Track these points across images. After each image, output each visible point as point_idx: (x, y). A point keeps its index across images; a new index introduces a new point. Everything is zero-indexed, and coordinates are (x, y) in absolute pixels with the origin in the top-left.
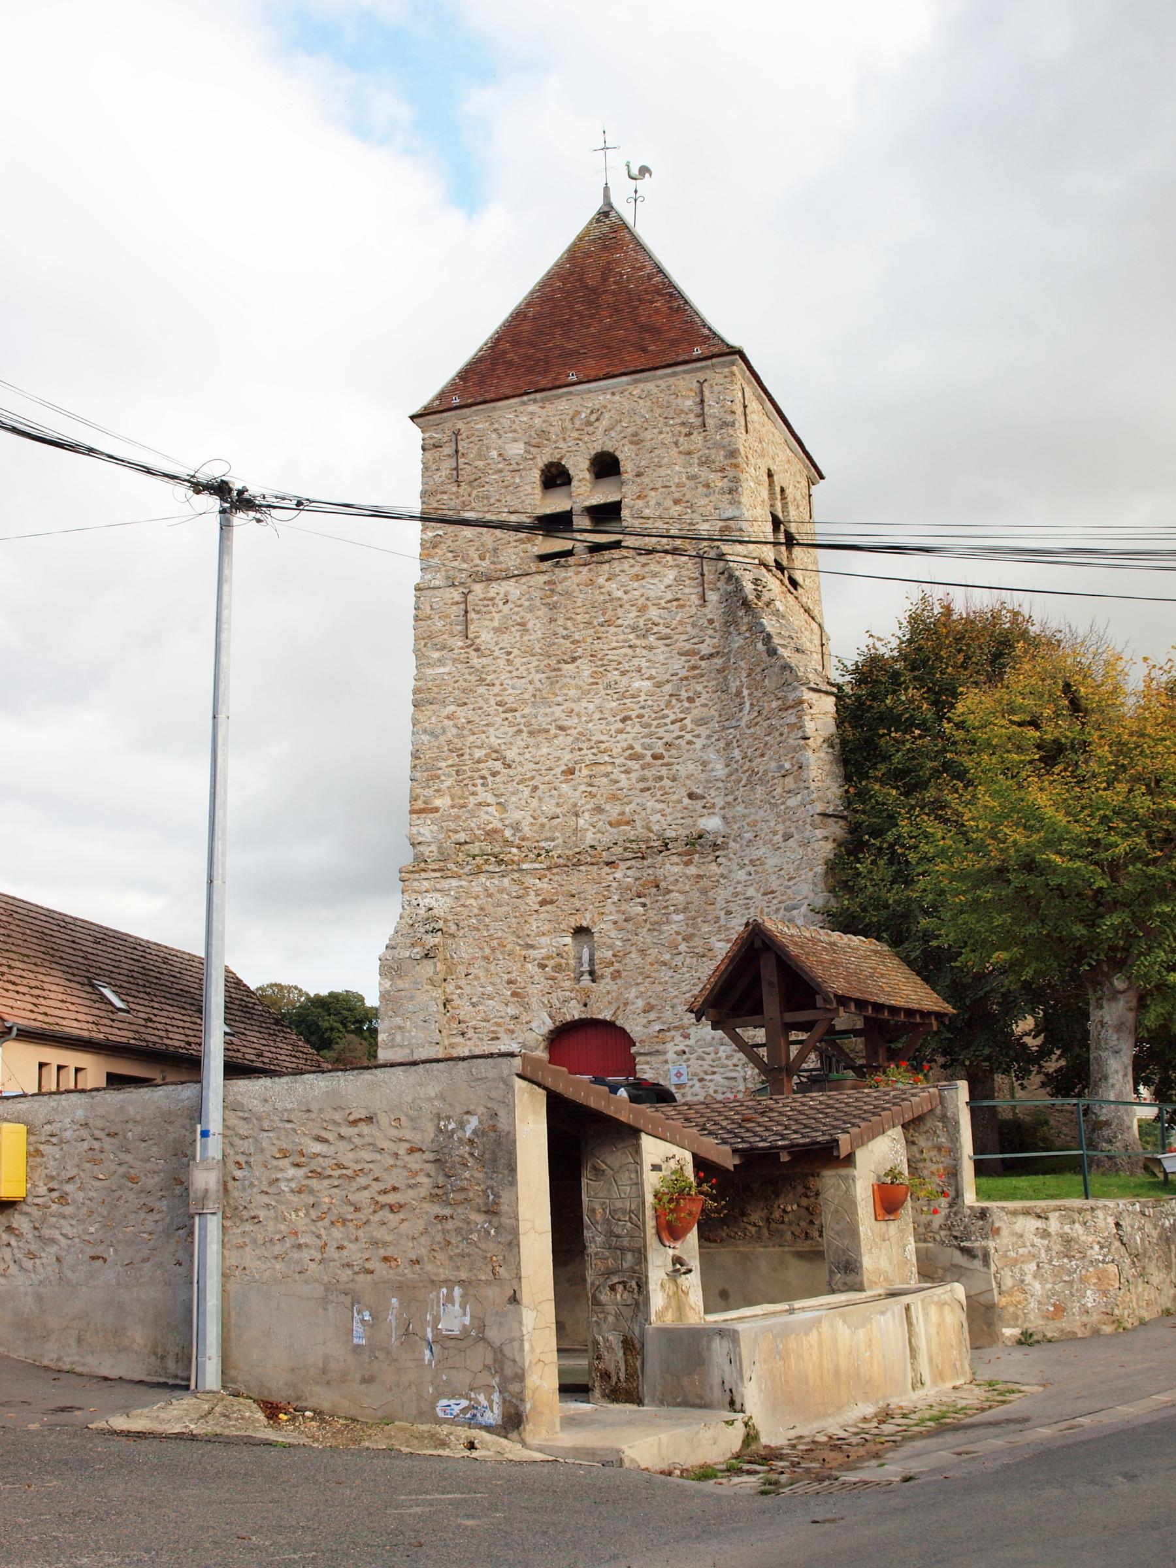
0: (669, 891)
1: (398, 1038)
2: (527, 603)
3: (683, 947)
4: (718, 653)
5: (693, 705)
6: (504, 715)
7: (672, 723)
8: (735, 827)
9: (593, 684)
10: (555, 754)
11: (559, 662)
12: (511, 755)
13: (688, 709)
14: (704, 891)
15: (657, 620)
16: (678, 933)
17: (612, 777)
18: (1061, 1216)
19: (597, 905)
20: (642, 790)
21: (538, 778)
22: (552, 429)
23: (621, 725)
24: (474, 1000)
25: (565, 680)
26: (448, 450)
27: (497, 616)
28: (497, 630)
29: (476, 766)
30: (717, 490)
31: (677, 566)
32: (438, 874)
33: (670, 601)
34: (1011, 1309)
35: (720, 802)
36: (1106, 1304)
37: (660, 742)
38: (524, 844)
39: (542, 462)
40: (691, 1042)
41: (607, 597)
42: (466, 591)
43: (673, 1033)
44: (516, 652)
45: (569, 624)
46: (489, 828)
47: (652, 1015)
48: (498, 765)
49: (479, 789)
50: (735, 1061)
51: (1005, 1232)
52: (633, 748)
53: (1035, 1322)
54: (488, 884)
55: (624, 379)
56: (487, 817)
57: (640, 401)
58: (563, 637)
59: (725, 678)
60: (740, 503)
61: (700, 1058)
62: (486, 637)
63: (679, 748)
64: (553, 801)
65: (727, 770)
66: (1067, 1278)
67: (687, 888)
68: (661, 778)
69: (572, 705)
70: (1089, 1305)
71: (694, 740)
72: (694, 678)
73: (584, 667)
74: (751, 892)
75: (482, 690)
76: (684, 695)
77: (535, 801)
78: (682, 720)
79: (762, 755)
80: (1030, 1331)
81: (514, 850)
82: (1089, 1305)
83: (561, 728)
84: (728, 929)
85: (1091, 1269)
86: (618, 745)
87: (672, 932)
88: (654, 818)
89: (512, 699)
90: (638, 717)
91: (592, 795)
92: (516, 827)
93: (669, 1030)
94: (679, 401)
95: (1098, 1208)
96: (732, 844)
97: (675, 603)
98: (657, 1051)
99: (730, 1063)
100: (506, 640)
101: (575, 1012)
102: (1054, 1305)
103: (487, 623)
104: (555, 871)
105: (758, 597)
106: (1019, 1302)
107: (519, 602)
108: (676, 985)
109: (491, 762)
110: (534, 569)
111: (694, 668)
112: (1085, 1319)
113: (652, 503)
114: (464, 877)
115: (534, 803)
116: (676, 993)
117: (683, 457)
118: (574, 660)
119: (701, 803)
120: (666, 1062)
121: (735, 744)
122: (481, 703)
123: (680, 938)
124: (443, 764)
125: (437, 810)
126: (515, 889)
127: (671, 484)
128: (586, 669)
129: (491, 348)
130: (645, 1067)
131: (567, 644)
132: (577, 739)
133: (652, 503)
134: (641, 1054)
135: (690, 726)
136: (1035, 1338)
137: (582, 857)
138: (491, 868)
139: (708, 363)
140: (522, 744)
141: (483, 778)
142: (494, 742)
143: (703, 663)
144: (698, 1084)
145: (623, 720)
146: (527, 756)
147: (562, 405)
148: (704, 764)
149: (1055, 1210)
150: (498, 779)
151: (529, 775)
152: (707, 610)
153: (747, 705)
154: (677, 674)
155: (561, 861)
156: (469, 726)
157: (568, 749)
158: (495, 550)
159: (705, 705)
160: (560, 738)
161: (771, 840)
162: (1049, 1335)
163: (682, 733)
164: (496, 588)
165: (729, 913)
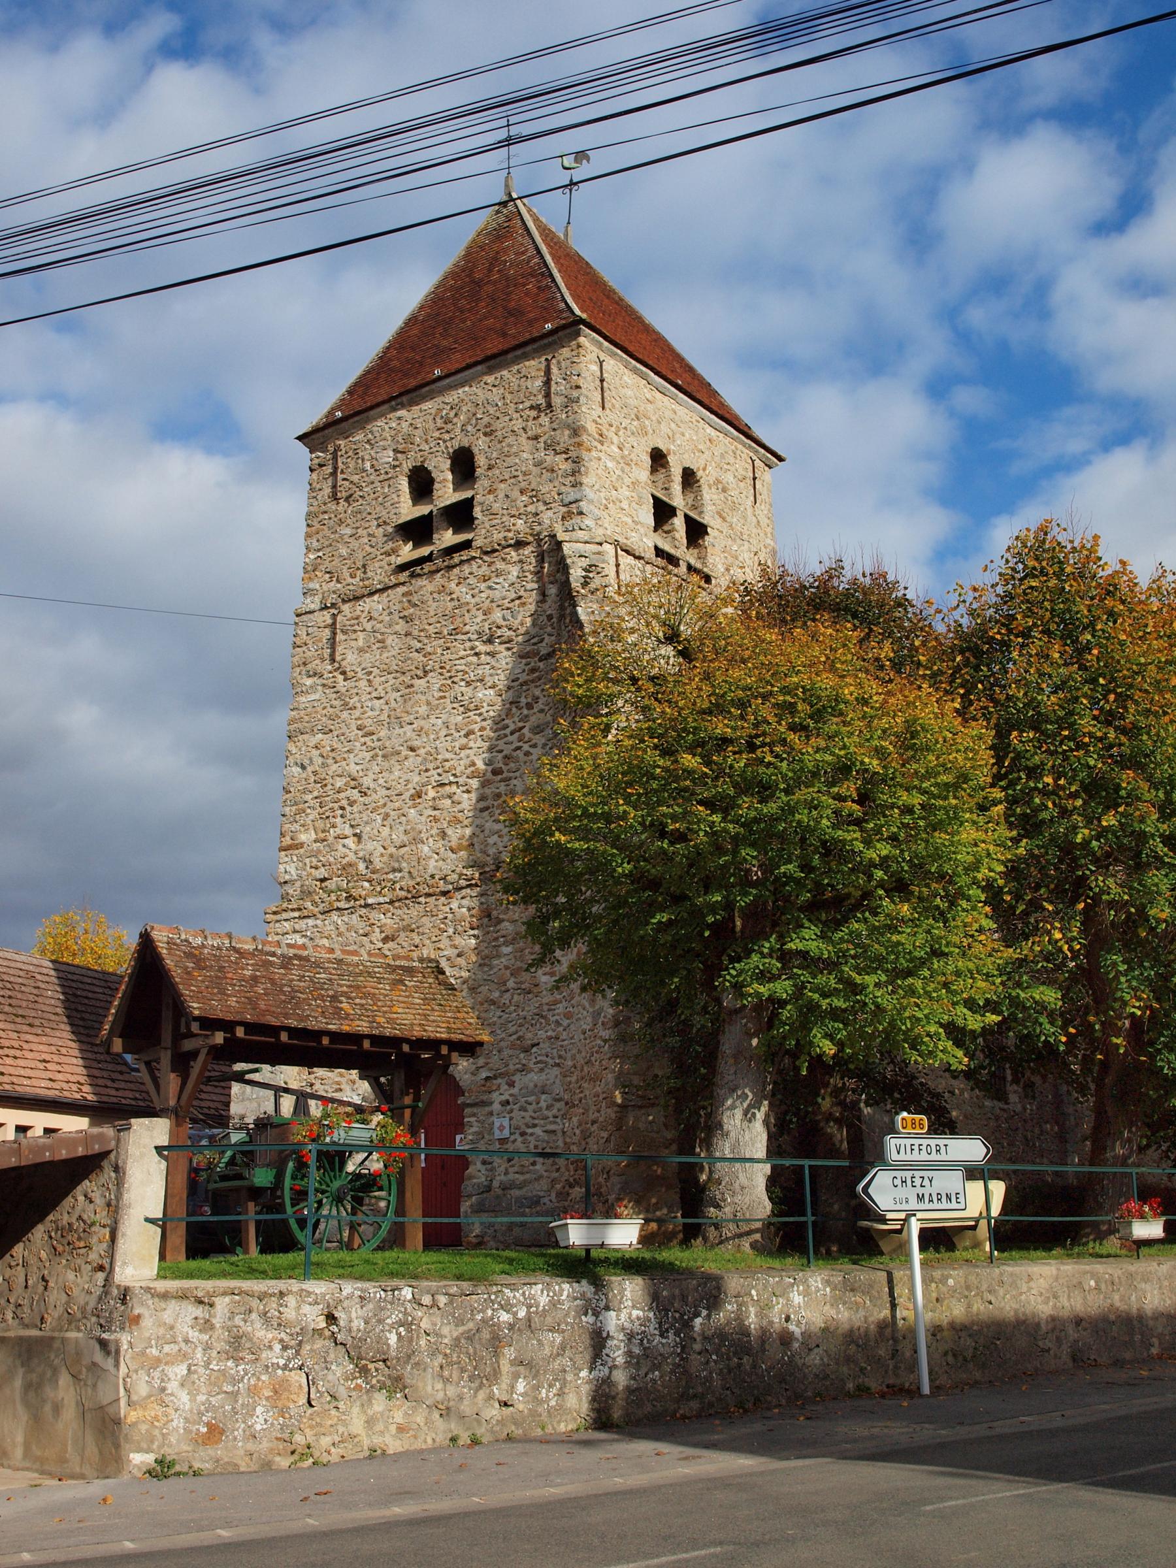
0: (500, 921)
5: (531, 712)
6: (363, 740)
7: (512, 733)
9: (441, 698)
12: (367, 781)
13: (526, 716)
15: (501, 622)
16: (507, 968)
17: (456, 798)
18: (233, 1302)
19: (434, 939)
21: (389, 804)
22: (416, 432)
25: (417, 697)
26: (328, 469)
27: (361, 635)
28: (361, 650)
29: (337, 796)
30: (560, 472)
31: (521, 561)
32: (296, 914)
33: (513, 601)
34: (143, 1428)
36: (283, 1427)
37: (500, 756)
38: (374, 876)
39: (407, 466)
40: (515, 1091)
41: (456, 603)
42: (336, 612)
43: (499, 1081)
46: (344, 861)
49: (339, 820)
50: (555, 1111)
51: (147, 1322)
52: (473, 764)
53: (177, 1446)
54: (339, 922)
55: (479, 368)
56: (344, 850)
57: (494, 389)
58: (417, 651)
60: (581, 484)
62: (350, 659)
64: (402, 829)
66: (230, 1389)
69: (422, 723)
70: (258, 1427)
71: (531, 750)
72: (533, 681)
73: (434, 681)
75: (345, 715)
76: (523, 701)
77: (387, 829)
78: (521, 729)
80: (169, 1458)
81: (366, 884)
82: (258, 1427)
85: (264, 1378)
86: (462, 762)
87: (501, 966)
90: (480, 730)
91: (436, 820)
92: (369, 862)
93: (495, 1077)
94: (529, 384)
95: (290, 1292)
97: (517, 602)
98: (482, 1102)
99: (550, 1114)
102: (208, 1424)
103: (353, 643)
104: (397, 904)
105: (585, 584)
106: (156, 1418)
110: (394, 581)
111: (533, 670)
112: (250, 1446)
114: (320, 916)
115: (386, 831)
116: (503, 1035)
117: (531, 442)
120: (491, 1114)
122: (344, 730)
123: (508, 972)
124: (309, 797)
125: (301, 845)
126: (362, 927)
127: (519, 473)
128: (435, 680)
129: (381, 358)
130: (472, 1119)
131: (419, 657)
132: (425, 759)
133: (501, 495)
136: (177, 1468)
137: (420, 888)
138: (342, 905)
139: (555, 337)
140: (377, 769)
141: (342, 808)
142: (353, 769)
143: (541, 665)
144: (520, 1139)
145: (467, 735)
146: (381, 781)
147: (427, 405)
149: (224, 1294)
150: (355, 808)
151: (382, 802)
152: (546, 606)
154: (517, 679)
155: (403, 894)
156: (333, 755)
157: (417, 770)
158: (364, 566)
159: (542, 711)
160: (411, 759)
162: (197, 1465)
163: (521, 744)
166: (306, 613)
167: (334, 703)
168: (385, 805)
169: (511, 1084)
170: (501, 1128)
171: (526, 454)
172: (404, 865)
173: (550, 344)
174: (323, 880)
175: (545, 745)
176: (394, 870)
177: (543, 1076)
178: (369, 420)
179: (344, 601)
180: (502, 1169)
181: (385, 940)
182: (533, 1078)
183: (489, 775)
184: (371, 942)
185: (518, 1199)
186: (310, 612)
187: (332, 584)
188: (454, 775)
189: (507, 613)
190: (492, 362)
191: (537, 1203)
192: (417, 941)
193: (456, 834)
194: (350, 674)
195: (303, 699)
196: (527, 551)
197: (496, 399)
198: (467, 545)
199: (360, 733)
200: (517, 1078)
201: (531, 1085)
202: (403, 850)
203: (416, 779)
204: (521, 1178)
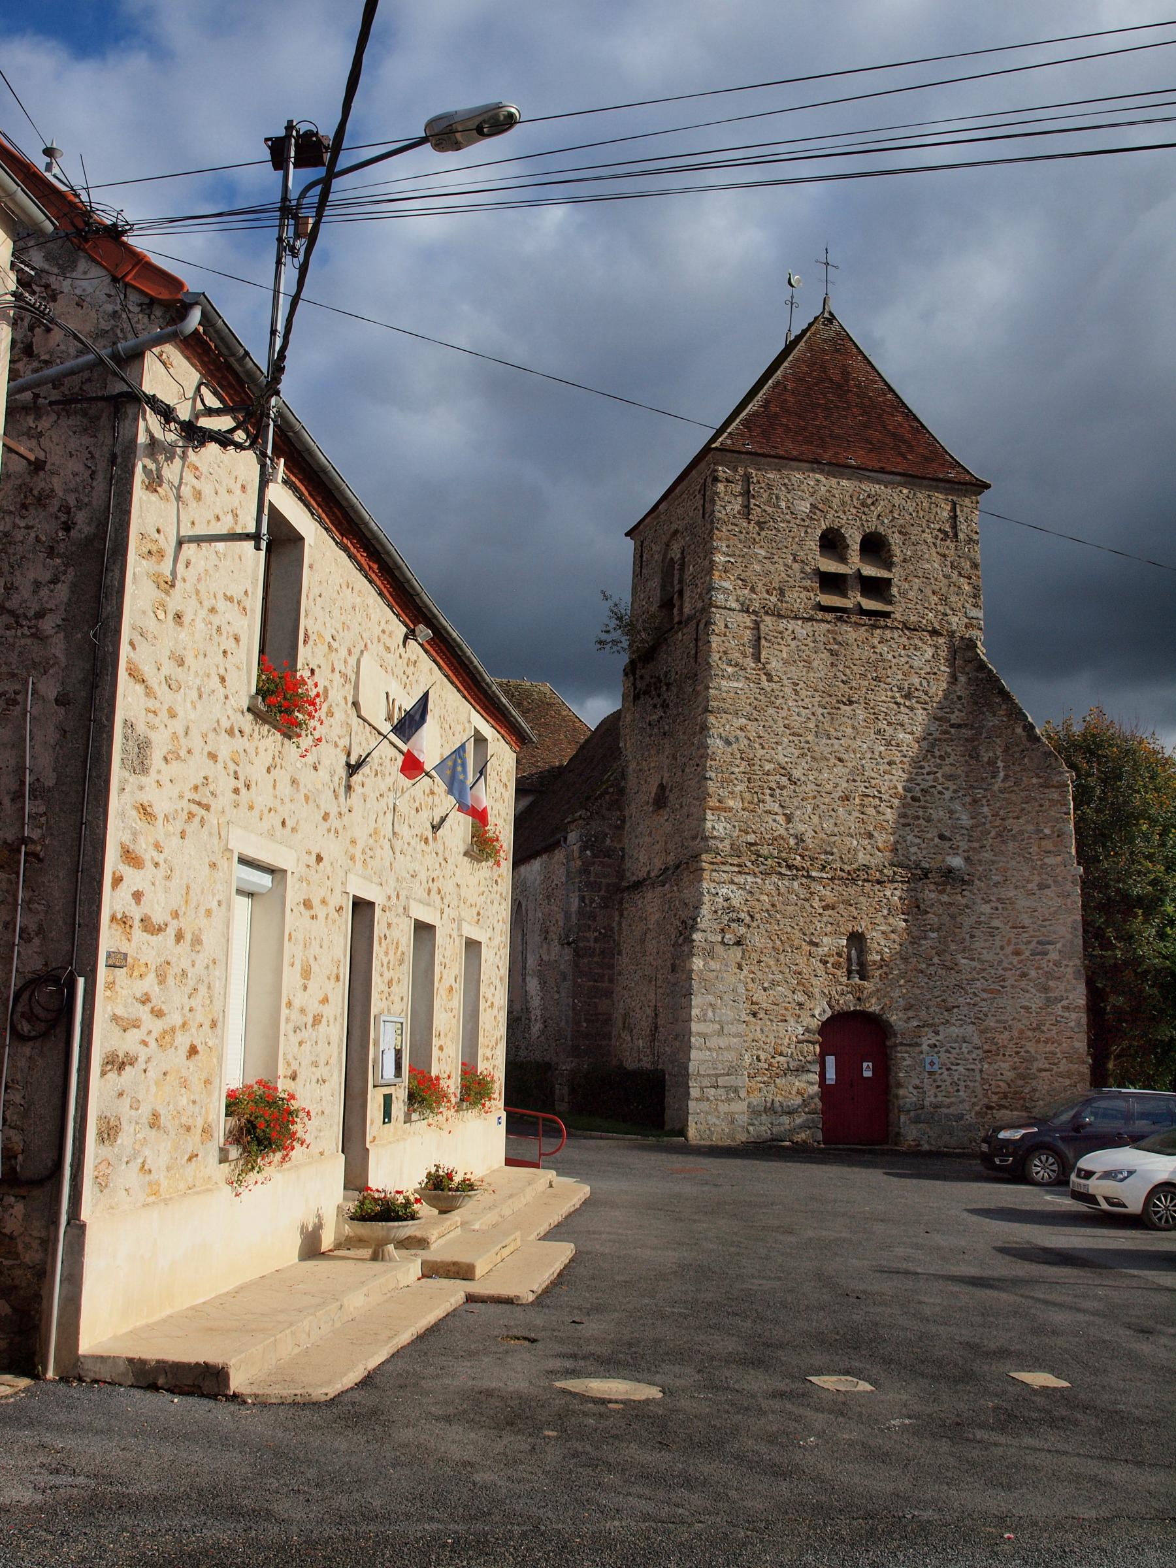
12: (797, 773)
27: (785, 649)
28: (785, 662)
32: (736, 869)
48: (784, 781)
50: (974, 1056)
55: (898, 478)
56: (774, 824)
58: (843, 682)
92: (800, 839)
101: (848, 1003)
111: (946, 732)
120: (922, 1052)
133: (915, 587)
138: (783, 870)
139: (964, 487)
143: (953, 730)
144: (946, 1073)
150: (784, 792)
164: (783, 624)
166: (725, 608)
168: (815, 797)
169: (937, 1033)
170: (932, 1063)
172: (835, 850)
174: (751, 844)
176: (826, 853)
178: (785, 467)
181: (825, 908)
182: (954, 1031)
183: (909, 800)
184: (812, 906)
185: (946, 1115)
186: (730, 609)
187: (746, 592)
188: (880, 792)
189: (924, 681)
190: (909, 479)
192: (855, 914)
193: (881, 838)
194: (775, 679)
196: (941, 640)
197: (911, 510)
198: (887, 615)
200: (941, 1028)
202: (833, 839)
203: (845, 785)
204: (948, 1100)
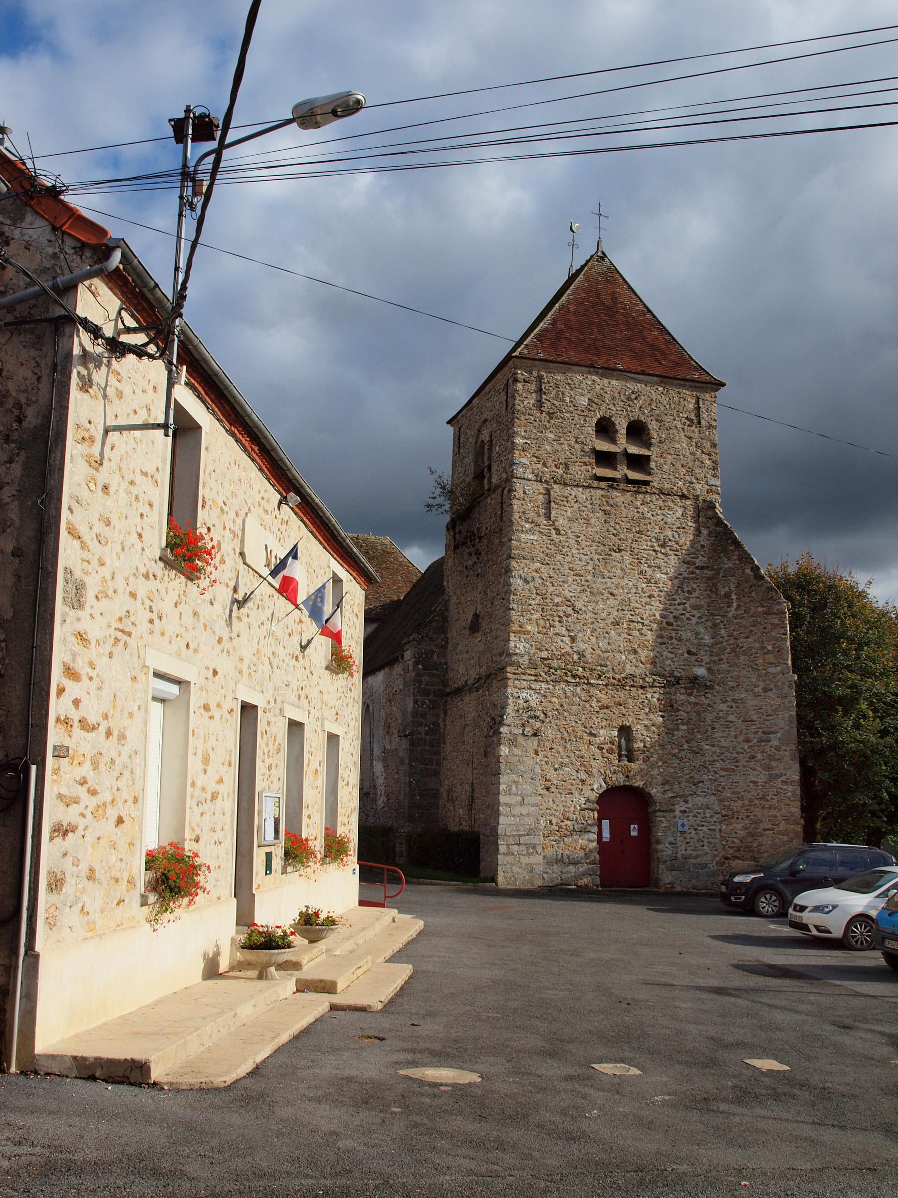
0: (678, 710)
1: (514, 788)
2: (590, 506)
3: (686, 746)
4: (708, 567)
8: (719, 677)
10: (607, 610)
11: (610, 550)
12: (579, 605)
14: (698, 713)
20: (660, 644)
21: (596, 623)
22: (606, 396)
23: (648, 600)
24: (556, 766)
27: (569, 510)
28: (570, 520)
29: (555, 608)
32: (533, 678)
35: (706, 659)
37: (671, 615)
40: (689, 805)
43: (678, 799)
44: (582, 537)
45: (617, 527)
47: (667, 787)
48: (570, 610)
50: (715, 819)
52: (655, 615)
55: (655, 379)
58: (613, 534)
59: (715, 585)
61: (695, 816)
62: (561, 522)
63: (682, 620)
65: (712, 641)
67: (689, 710)
68: (671, 638)
74: (731, 718)
75: (559, 557)
76: (686, 589)
79: (747, 638)
83: (612, 594)
84: (712, 738)
88: (668, 662)
89: (580, 568)
92: (582, 655)
93: (676, 797)
96: (717, 687)
100: (577, 527)
101: (619, 779)
107: (585, 504)
108: (681, 769)
109: (565, 607)
111: (693, 573)
113: (669, 462)
118: (620, 551)
119: (694, 658)
120: (675, 817)
121: (722, 625)
126: (584, 696)
133: (669, 462)
134: (660, 811)
135: (689, 609)
140: (587, 600)
142: (569, 595)
143: (698, 571)
145: (650, 597)
148: (697, 634)
150: (570, 619)
153: (735, 605)
161: (752, 690)
164: (568, 490)
165: (713, 728)
167: (550, 547)
168: (593, 623)
171: (683, 445)
172: (608, 663)
173: (699, 387)
175: (700, 618)
177: (706, 800)
178: (569, 370)
179: (555, 482)
180: (683, 847)
182: (700, 800)
184: (591, 706)
185: (694, 865)
186: (527, 480)
188: (642, 619)
190: (664, 380)
191: (705, 867)
193: (643, 654)
194: (562, 532)
195: (523, 536)
196: (688, 503)
197: (665, 403)
198: (647, 483)
199: (572, 573)
200: (690, 798)
201: (700, 804)
202: (607, 654)
204: (696, 853)
